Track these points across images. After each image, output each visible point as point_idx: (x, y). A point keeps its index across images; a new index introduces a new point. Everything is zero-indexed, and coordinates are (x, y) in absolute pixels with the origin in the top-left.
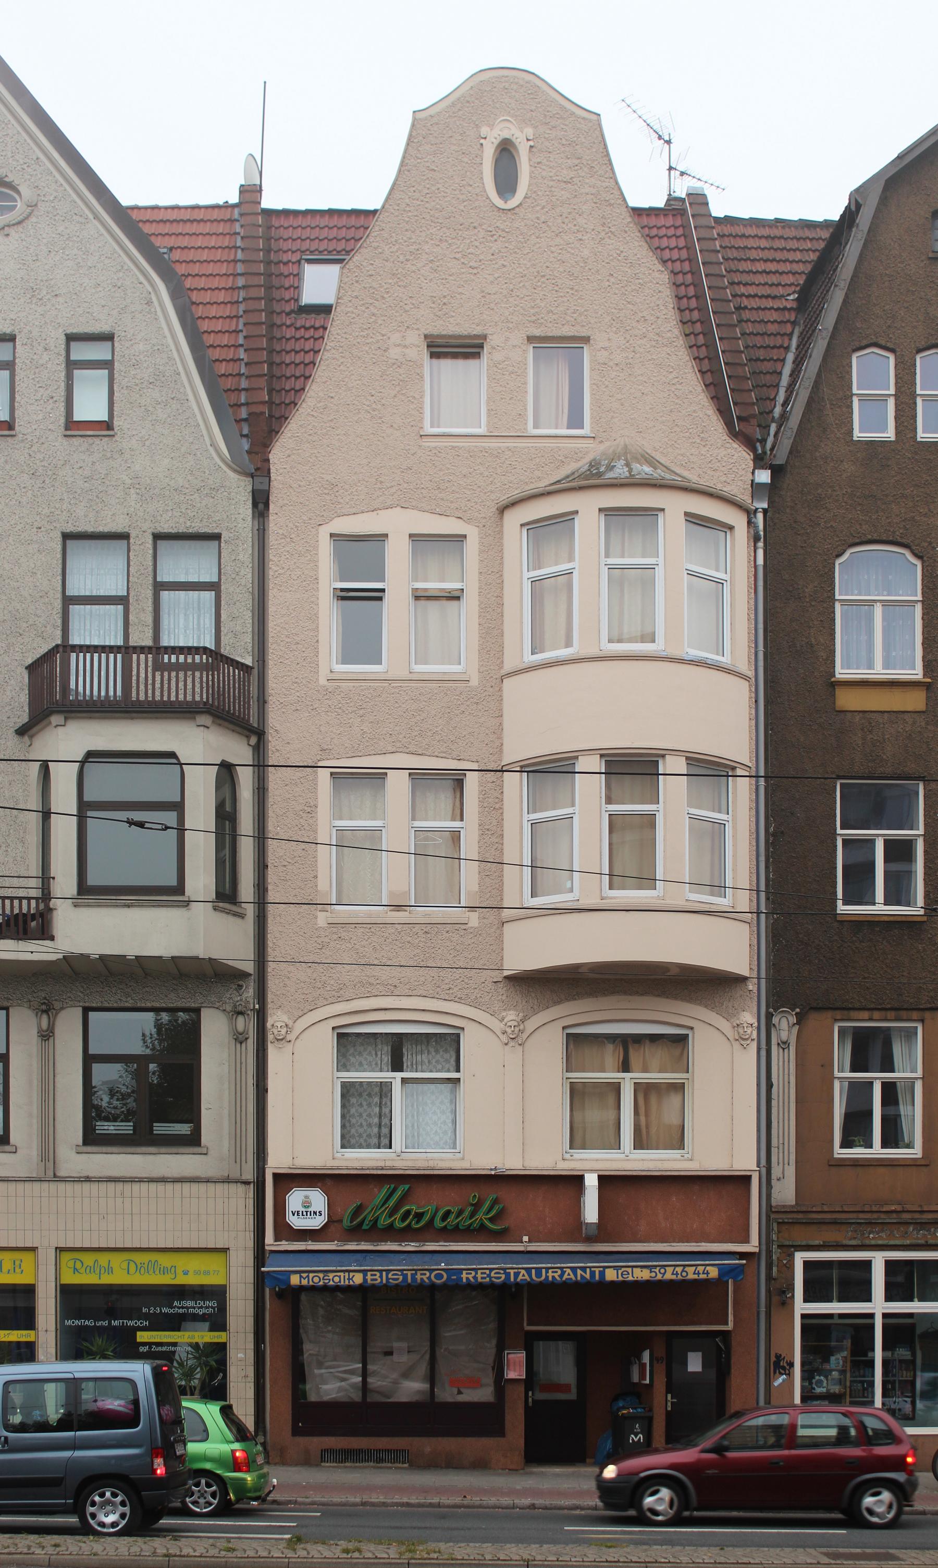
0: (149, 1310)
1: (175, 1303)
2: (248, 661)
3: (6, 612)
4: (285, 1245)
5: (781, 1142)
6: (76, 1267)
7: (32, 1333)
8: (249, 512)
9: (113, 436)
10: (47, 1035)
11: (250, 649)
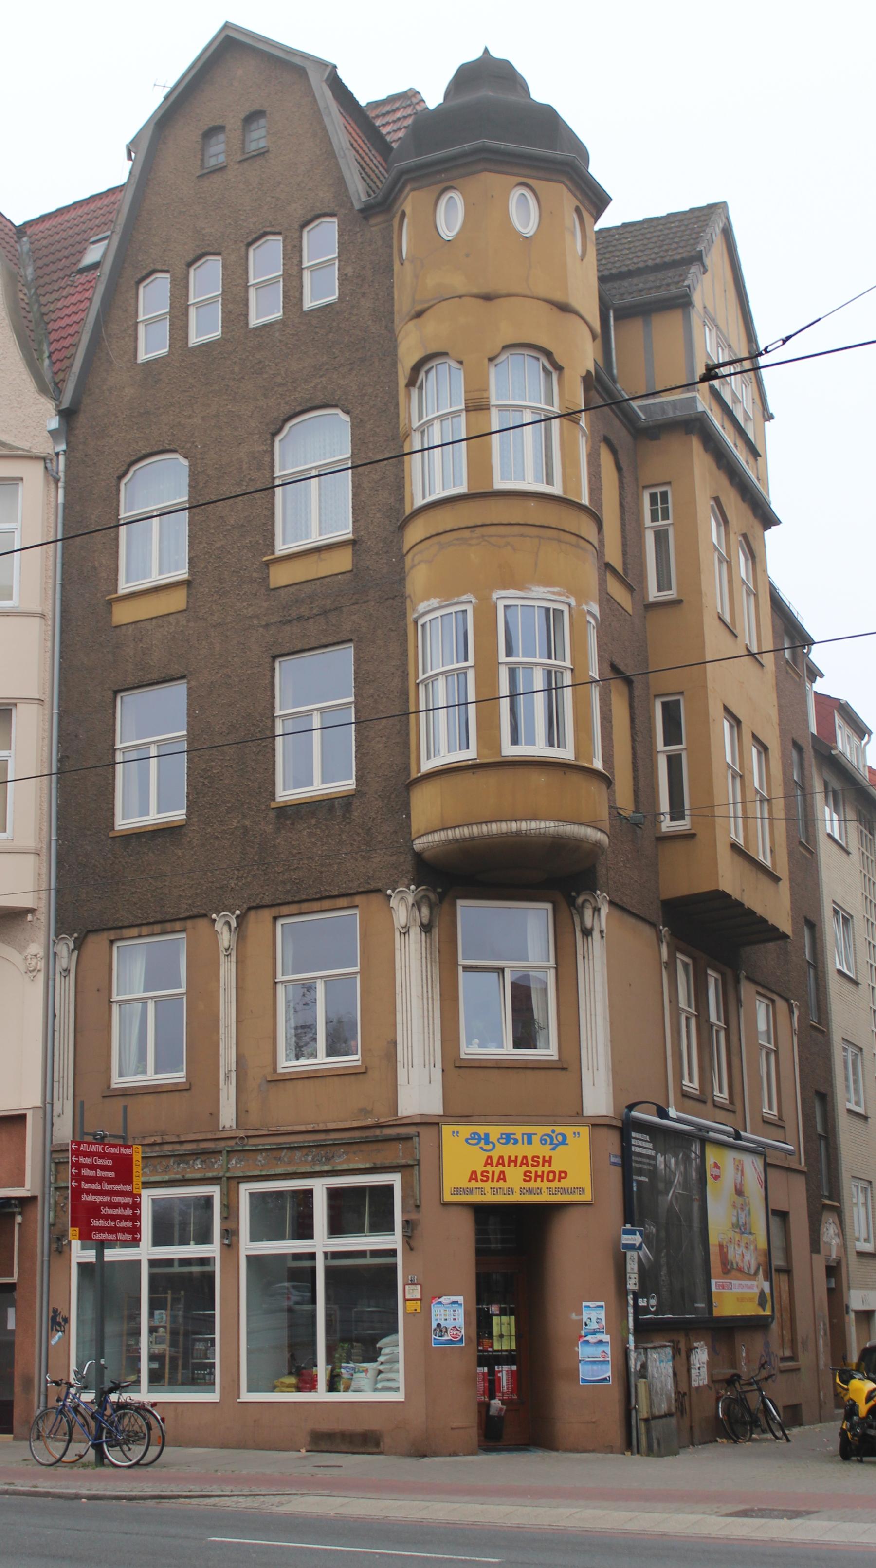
5: (61, 1076)
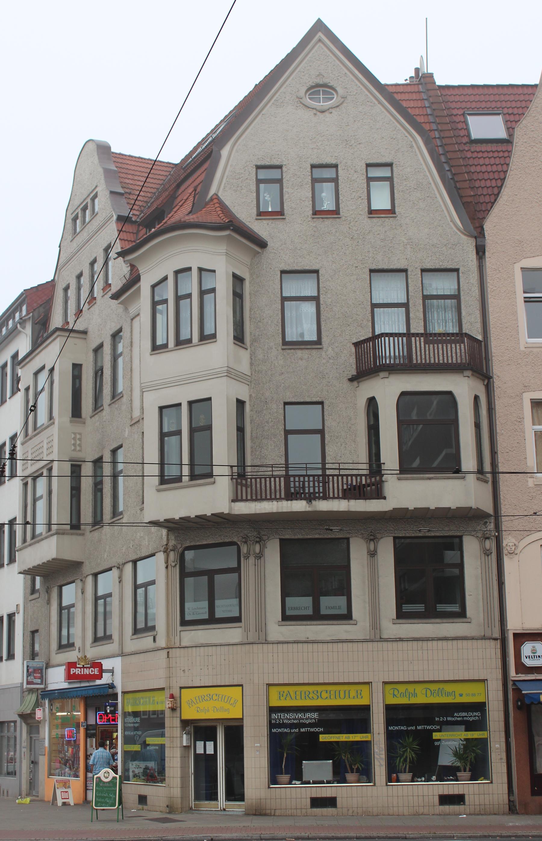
0: (440, 719)
1: (455, 714)
2: (480, 337)
3: (340, 313)
4: (522, 677)
6: (395, 693)
7: (369, 735)
8: (475, 256)
9: (396, 217)
10: (373, 554)
11: (480, 331)
